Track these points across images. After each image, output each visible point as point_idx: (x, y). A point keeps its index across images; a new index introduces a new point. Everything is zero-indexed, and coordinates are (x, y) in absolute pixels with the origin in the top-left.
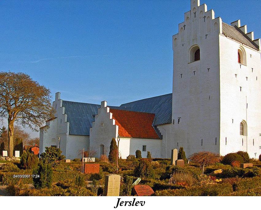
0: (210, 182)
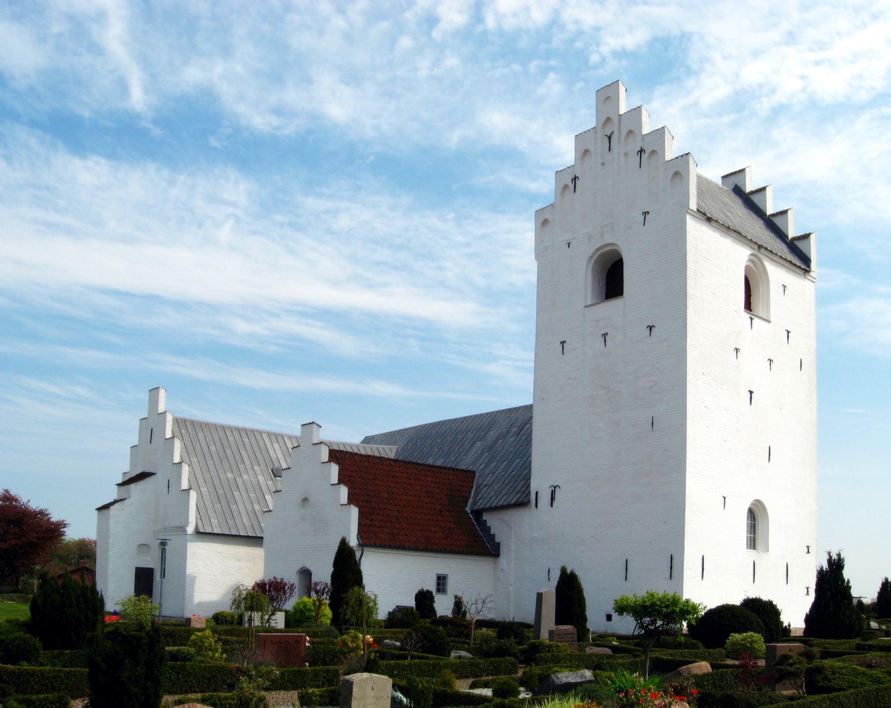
0: (324, 677)
